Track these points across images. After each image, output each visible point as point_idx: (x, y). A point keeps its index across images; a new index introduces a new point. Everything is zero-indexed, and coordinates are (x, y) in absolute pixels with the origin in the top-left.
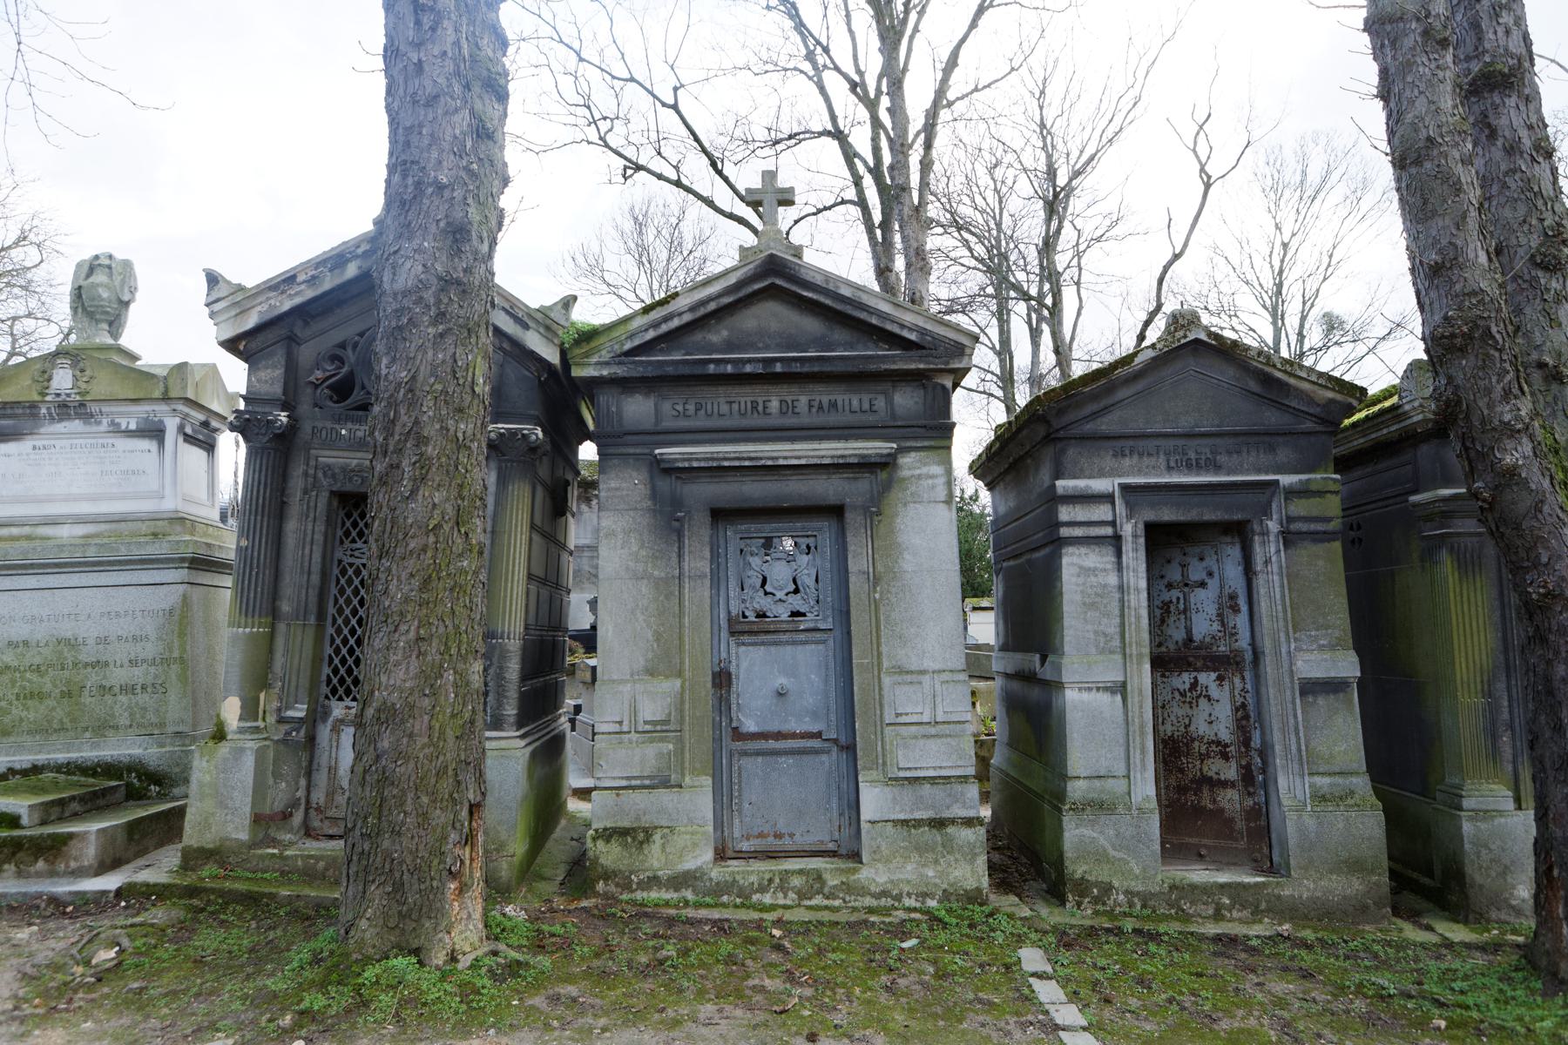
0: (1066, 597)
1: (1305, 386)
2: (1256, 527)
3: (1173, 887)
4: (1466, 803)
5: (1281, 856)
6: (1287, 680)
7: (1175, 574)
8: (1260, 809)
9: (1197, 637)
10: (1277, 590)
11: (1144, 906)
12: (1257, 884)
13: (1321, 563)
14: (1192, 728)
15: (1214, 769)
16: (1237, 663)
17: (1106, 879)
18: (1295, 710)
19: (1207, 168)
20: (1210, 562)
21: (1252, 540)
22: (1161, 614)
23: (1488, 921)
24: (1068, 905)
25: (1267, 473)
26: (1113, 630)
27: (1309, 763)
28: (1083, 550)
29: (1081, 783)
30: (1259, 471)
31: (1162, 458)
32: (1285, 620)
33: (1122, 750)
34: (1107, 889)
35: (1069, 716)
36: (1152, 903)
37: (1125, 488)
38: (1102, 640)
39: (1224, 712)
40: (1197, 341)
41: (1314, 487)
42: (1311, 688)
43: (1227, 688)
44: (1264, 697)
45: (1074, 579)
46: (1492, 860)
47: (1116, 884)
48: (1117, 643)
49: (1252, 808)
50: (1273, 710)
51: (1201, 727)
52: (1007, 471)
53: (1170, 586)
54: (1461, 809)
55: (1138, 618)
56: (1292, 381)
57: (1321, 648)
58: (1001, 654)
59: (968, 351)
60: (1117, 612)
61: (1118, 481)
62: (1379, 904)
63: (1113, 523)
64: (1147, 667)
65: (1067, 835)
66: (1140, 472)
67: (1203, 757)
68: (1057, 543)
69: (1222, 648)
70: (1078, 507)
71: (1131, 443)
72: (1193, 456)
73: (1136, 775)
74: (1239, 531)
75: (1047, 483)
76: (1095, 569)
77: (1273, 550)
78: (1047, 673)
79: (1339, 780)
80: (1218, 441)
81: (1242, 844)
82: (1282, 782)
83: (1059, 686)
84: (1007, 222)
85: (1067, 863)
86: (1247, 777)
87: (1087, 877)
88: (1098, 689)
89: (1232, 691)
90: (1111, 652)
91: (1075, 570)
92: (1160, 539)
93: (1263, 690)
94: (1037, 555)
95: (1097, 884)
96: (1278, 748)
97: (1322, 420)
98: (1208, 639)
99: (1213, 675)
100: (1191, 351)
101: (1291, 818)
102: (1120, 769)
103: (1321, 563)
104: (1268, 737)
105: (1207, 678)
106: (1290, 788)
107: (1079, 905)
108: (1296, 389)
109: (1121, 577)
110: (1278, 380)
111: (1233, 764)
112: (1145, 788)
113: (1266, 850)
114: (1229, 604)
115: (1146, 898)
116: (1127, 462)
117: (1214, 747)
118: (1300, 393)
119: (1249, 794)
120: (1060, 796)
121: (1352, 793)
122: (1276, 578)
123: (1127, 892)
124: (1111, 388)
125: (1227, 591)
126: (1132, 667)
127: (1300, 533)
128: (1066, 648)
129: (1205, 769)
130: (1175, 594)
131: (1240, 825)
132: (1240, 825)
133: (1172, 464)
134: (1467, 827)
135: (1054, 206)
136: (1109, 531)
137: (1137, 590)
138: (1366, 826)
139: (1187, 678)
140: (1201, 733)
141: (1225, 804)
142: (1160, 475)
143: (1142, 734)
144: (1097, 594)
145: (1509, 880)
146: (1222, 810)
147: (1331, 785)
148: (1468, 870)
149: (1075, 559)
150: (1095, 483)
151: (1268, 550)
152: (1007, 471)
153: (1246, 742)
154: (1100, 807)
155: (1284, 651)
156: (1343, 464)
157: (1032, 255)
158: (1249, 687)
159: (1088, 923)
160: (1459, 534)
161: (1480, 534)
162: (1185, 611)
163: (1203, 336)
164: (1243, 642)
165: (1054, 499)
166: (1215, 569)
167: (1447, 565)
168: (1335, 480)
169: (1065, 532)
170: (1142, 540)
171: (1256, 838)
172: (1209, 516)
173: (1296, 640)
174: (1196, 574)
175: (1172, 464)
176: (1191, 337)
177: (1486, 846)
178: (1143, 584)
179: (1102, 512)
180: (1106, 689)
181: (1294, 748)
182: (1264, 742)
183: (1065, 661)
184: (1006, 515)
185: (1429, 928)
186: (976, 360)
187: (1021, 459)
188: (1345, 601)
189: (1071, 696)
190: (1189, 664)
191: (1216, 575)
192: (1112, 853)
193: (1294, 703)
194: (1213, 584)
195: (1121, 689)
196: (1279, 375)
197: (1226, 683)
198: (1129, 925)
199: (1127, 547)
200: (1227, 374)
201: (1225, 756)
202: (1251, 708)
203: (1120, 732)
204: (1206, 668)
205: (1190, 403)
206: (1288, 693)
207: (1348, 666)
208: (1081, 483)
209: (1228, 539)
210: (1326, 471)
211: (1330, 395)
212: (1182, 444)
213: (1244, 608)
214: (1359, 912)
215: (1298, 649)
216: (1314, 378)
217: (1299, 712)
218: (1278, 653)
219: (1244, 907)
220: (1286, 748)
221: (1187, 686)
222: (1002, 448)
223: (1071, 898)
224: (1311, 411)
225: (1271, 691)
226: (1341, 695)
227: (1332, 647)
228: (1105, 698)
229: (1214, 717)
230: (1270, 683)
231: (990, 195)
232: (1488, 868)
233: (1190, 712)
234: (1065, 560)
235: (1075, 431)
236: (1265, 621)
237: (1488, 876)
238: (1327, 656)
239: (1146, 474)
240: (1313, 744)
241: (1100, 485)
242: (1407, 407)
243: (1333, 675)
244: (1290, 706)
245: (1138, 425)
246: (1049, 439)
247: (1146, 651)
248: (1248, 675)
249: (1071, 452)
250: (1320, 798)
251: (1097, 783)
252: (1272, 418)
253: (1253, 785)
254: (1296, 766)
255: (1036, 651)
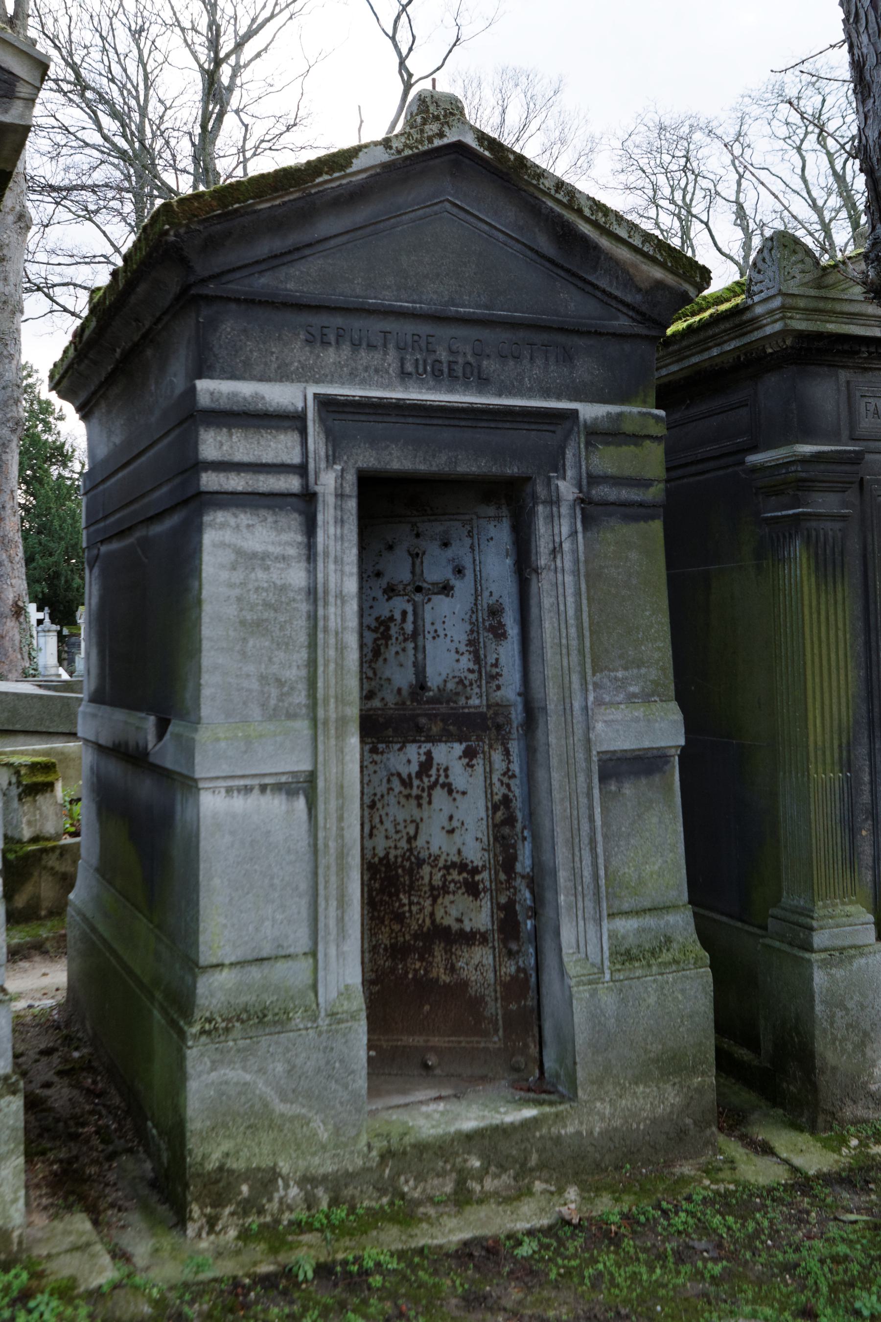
0: (208, 610)
1: (623, 254)
2: (541, 491)
3: (386, 1155)
4: (819, 939)
5: (561, 1060)
6: (581, 755)
7: (399, 570)
8: (527, 979)
9: (434, 680)
10: (570, 600)
11: (335, 1202)
12: (526, 1124)
13: (633, 555)
14: (420, 842)
15: (454, 913)
16: (499, 727)
17: (266, 1162)
18: (591, 807)
19: (408, 63)
20: (460, 550)
21: (533, 513)
22: (377, 637)
23: (842, 1123)
24: (191, 1230)
25: (559, 398)
26: (295, 673)
27: (608, 898)
28: (244, 518)
29: (224, 978)
30: (546, 393)
31: (392, 357)
32: (581, 652)
33: (304, 903)
34: (266, 1180)
35: (206, 845)
36: (348, 1192)
37: (326, 404)
38: (274, 692)
39: (473, 812)
40: (459, 147)
41: (628, 427)
42: (617, 768)
43: (479, 769)
44: (543, 787)
45: (224, 575)
46: (849, 1026)
47: (284, 1167)
48: (300, 697)
49: (514, 978)
50: (557, 809)
51: (435, 841)
52: (110, 380)
53: (391, 591)
54: (810, 949)
55: (341, 648)
56: (604, 242)
57: (631, 698)
58: (92, 708)
59: (23, 90)
60: (302, 638)
61: (312, 389)
62: (701, 1124)
63: (302, 470)
64: (354, 741)
65: (193, 1085)
66: (353, 377)
67: (437, 893)
68: (195, 503)
69: (475, 701)
70: (237, 435)
71: (338, 321)
72: (443, 355)
73: (328, 950)
74: (511, 498)
75: (180, 384)
76: (264, 556)
77: (565, 530)
78: (167, 755)
79: (649, 921)
80: (485, 334)
81: (496, 1041)
82: (567, 935)
83: (189, 784)
84: (154, 110)
85: (192, 1143)
86: (508, 924)
87: (232, 1164)
88: (263, 788)
89: (488, 775)
90: (291, 716)
91: (227, 557)
92: (386, 505)
93: (541, 774)
94: (157, 529)
95: (248, 1175)
96: (563, 875)
97: (643, 317)
98: (451, 686)
99: (458, 748)
100: (450, 166)
101: (581, 994)
102: (300, 940)
103: (633, 555)
104: (546, 857)
105: (448, 754)
106: (580, 941)
107: (212, 1222)
108: (610, 258)
109: (312, 572)
110: (584, 239)
111: (486, 903)
112: (344, 971)
113: (533, 1050)
114: (487, 624)
115: (336, 1185)
116: (330, 356)
117: (455, 875)
118: (614, 265)
119: (511, 954)
120: (181, 1003)
121: (669, 940)
122: (569, 579)
123: (307, 1181)
124: (308, 211)
125: (486, 601)
126: (327, 744)
127: (606, 504)
128: (206, 711)
129: (439, 913)
130: (399, 604)
131: (493, 1008)
132: (493, 1008)
133: (409, 368)
134: (819, 978)
135: (215, 93)
136: (293, 483)
137: (341, 597)
138: (686, 994)
139: (414, 753)
140: (434, 850)
141: (471, 975)
142: (388, 386)
143: (342, 868)
144: (267, 605)
145: (869, 1053)
146: (464, 984)
147: (641, 931)
148: (819, 1046)
149: (228, 536)
150: (270, 392)
151: (558, 531)
152: (110, 380)
153: (508, 864)
154: (259, 1019)
155: (577, 705)
156: (666, 396)
157: (185, 149)
158: (515, 767)
159: (227, 1268)
160: (818, 516)
161: (844, 518)
162: (415, 635)
163: (470, 140)
164: (510, 689)
165: (193, 417)
166: (467, 562)
167: (799, 565)
168: (657, 418)
169: (210, 481)
170: (352, 504)
171: (515, 1036)
172: (468, 466)
173: (596, 686)
174: (435, 571)
175: (409, 368)
176: (451, 137)
177: (842, 1006)
178: (351, 586)
179: (281, 447)
180: (278, 788)
181: (587, 873)
182: (537, 863)
183: (203, 736)
184: (106, 461)
185: (766, 1150)
186: (39, 114)
187: (133, 353)
188: (665, 619)
189: (212, 804)
190: (419, 729)
191: (469, 573)
192: (280, 1107)
193: (589, 795)
194: (463, 588)
195: (306, 786)
196: (586, 229)
197: (478, 762)
198: (305, 1256)
199: (326, 515)
200: (505, 216)
201: (473, 890)
202: (517, 804)
203: (303, 868)
204: (447, 737)
205: (441, 258)
206: (582, 778)
207: (664, 729)
208: (245, 389)
209: (491, 511)
210: (644, 403)
211: (658, 273)
212: (426, 331)
213: (513, 630)
214: (676, 1138)
215: (599, 702)
216: (637, 241)
217: (598, 811)
218: (567, 711)
219: (503, 1168)
220: (576, 875)
221: (414, 768)
222: (101, 330)
223: (195, 1210)
224: (629, 299)
225: (555, 775)
226: (657, 778)
227: (646, 698)
228: (275, 804)
229: (458, 825)
230: (554, 761)
231: (132, 66)
232: (844, 1039)
233: (416, 813)
234: (209, 538)
235: (238, 286)
236: (549, 653)
237: (844, 1051)
238: (639, 713)
239: (363, 383)
240: (614, 863)
241: (281, 395)
242: (759, 310)
243: (647, 744)
244: (583, 800)
245: (354, 289)
246: (188, 299)
247: (353, 711)
248: (514, 747)
249: (229, 327)
250: (625, 956)
251: (255, 973)
252: (572, 304)
253: (517, 938)
254: (589, 905)
255: (150, 710)
